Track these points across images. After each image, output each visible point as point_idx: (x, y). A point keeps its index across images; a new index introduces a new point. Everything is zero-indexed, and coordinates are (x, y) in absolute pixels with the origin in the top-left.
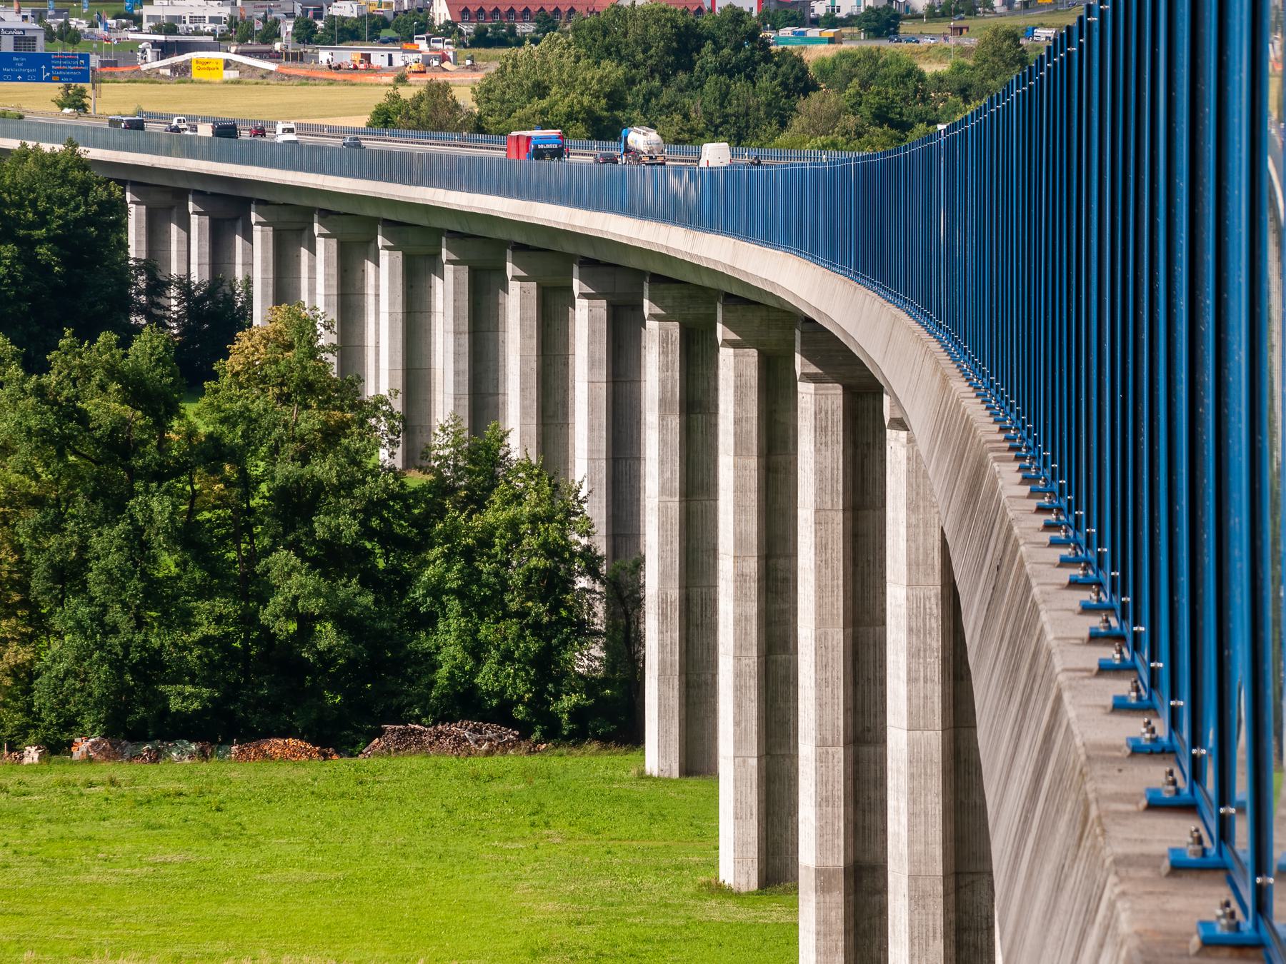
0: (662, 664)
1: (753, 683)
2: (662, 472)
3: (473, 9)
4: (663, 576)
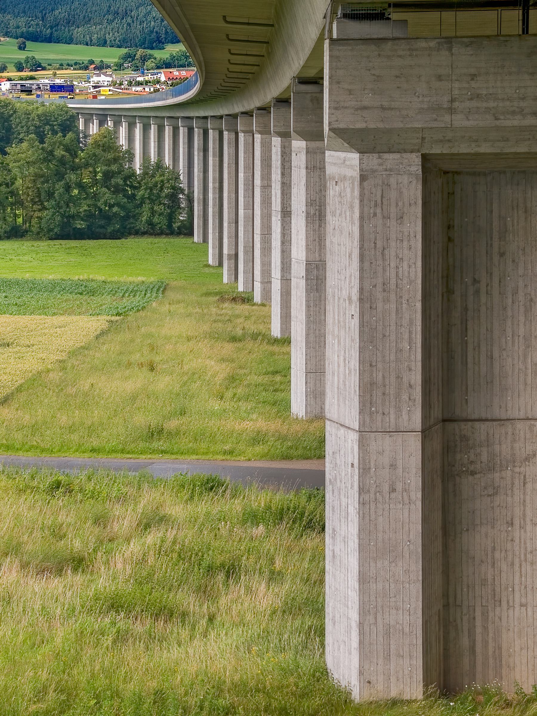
0: (198, 214)
1: (217, 214)
2: (198, 167)
3: (171, 78)
4: (199, 193)
